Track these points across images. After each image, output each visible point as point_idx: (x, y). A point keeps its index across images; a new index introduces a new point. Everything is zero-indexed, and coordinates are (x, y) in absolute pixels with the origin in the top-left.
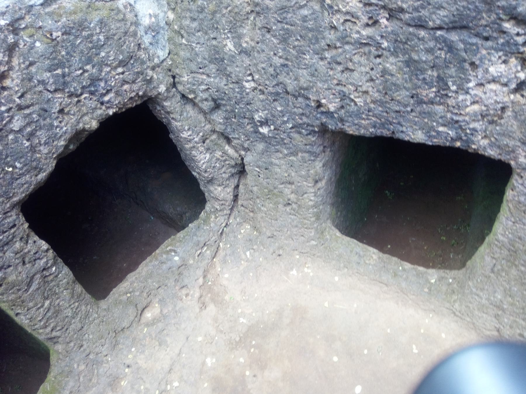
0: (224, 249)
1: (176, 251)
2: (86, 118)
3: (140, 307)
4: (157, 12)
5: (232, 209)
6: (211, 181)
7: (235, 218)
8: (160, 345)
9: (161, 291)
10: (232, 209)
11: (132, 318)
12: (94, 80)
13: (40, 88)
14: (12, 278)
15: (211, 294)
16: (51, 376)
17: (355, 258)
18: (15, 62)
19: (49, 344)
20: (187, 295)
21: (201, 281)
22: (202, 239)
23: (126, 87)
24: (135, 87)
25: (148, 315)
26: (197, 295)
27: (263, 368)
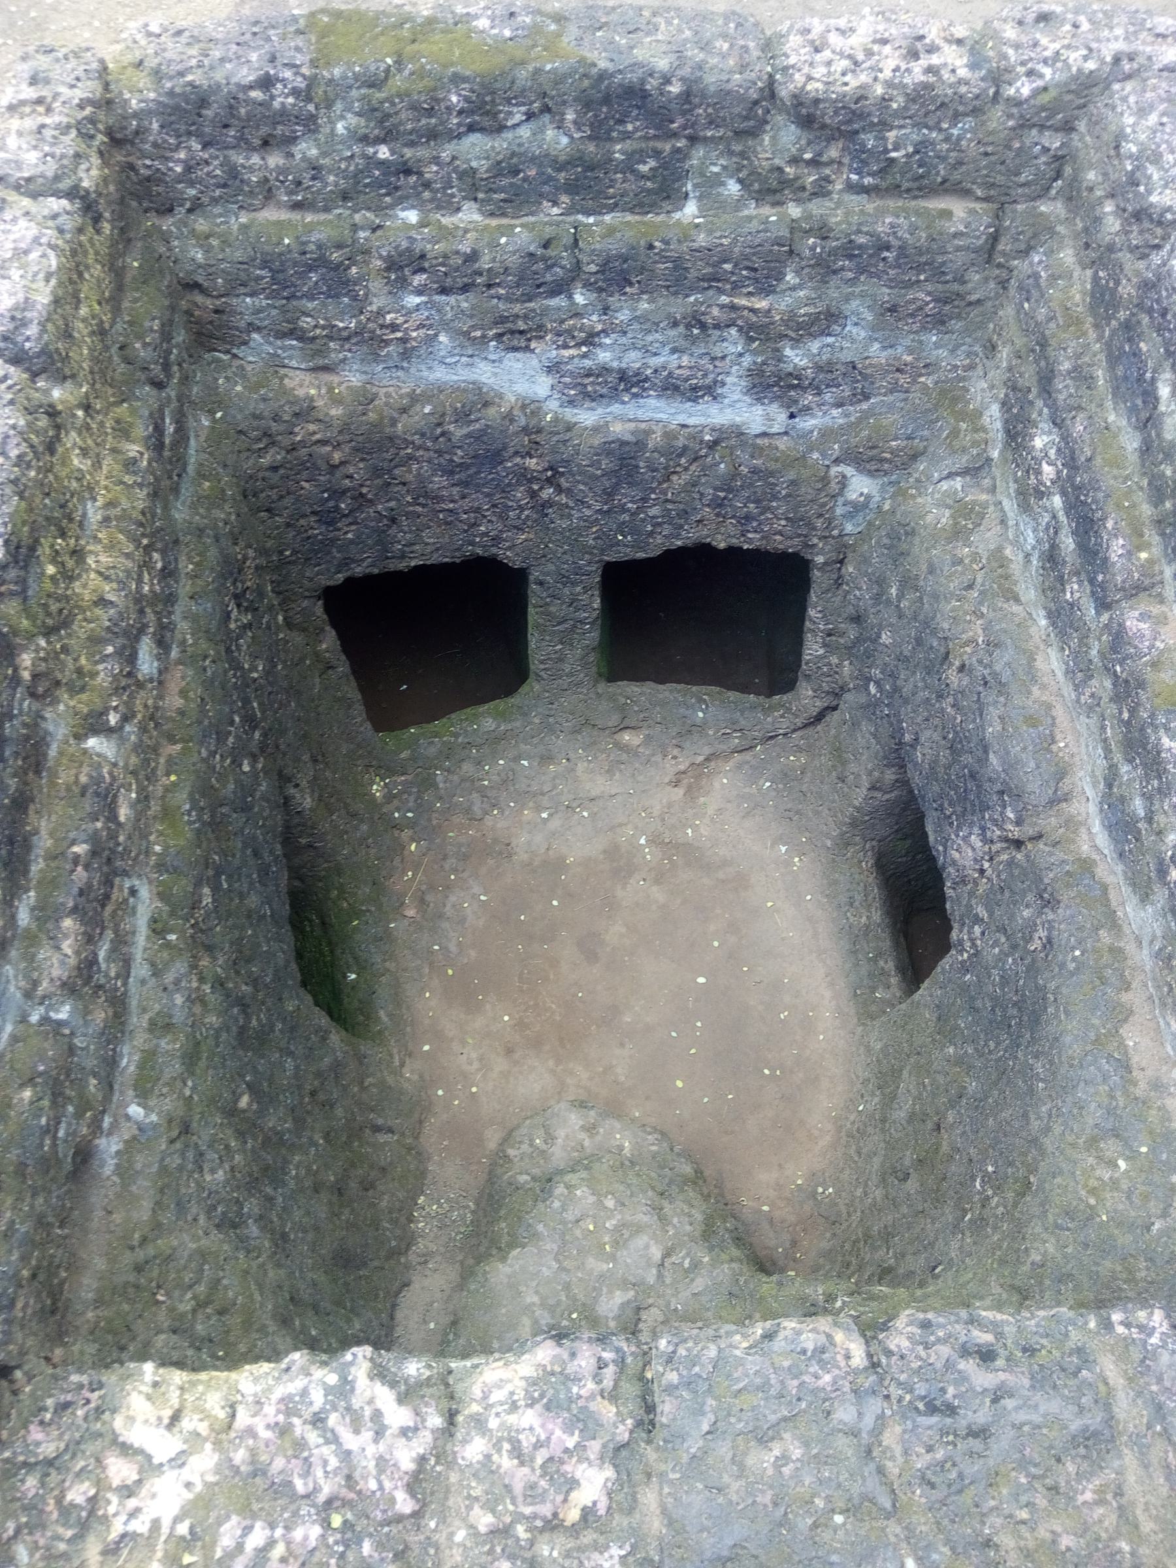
0: (755, 756)
1: (706, 706)
2: (719, 537)
3: (626, 723)
4: (874, 493)
5: (805, 726)
6: (808, 677)
7: (802, 738)
8: (608, 771)
9: (658, 728)
10: (805, 726)
11: (610, 724)
12: (748, 518)
13: (697, 496)
14: (553, 609)
15: (692, 780)
16: (511, 701)
17: (843, 899)
18: (693, 468)
19: (532, 675)
20: (674, 758)
21: (700, 759)
22: (743, 723)
23: (778, 537)
24: (789, 543)
25: (626, 737)
26: (682, 767)
27: (657, 881)
